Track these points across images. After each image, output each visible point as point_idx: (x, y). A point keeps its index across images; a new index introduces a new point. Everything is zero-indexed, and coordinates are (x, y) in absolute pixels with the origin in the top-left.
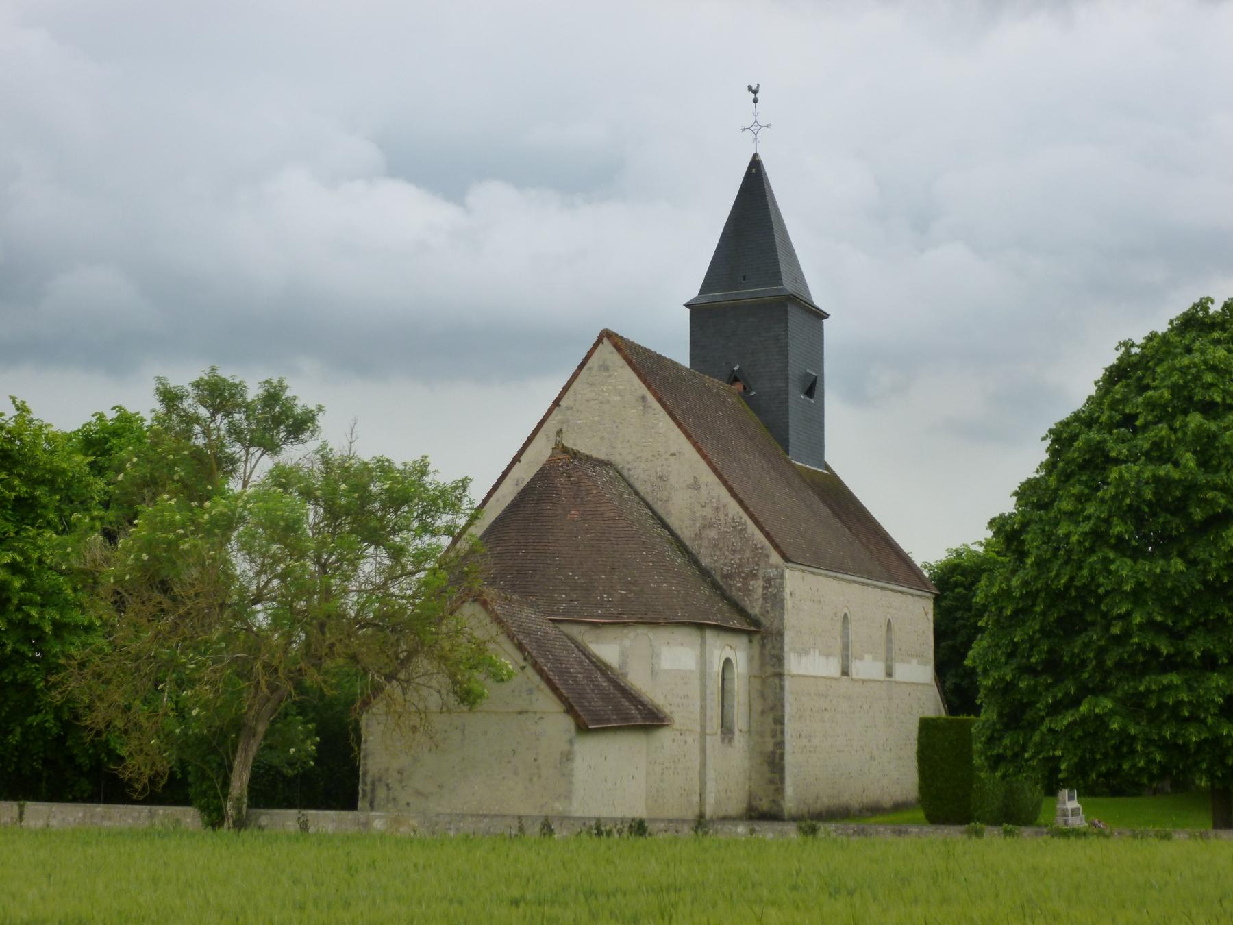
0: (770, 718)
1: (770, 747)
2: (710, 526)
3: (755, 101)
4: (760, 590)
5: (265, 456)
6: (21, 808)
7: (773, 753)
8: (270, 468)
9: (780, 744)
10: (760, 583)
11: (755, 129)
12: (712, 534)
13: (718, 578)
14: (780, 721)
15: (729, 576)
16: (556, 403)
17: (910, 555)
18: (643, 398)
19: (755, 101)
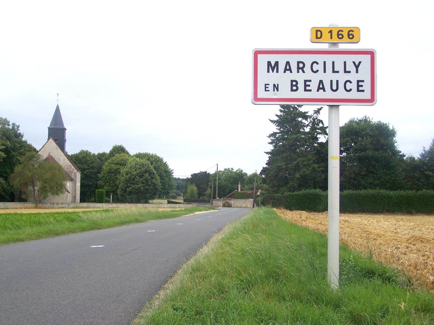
0: (74, 192)
1: (74, 195)
2: (66, 166)
3: (58, 96)
4: (73, 175)
5: (255, 172)
6: (424, 151)
7: (74, 196)
8: (221, 170)
9: (76, 195)
10: (73, 174)
11: (58, 100)
12: (67, 167)
13: (67, 173)
14: (76, 192)
15: (69, 173)
16: (43, 147)
17: (221, 169)
18: (57, 147)
19: (58, 96)
